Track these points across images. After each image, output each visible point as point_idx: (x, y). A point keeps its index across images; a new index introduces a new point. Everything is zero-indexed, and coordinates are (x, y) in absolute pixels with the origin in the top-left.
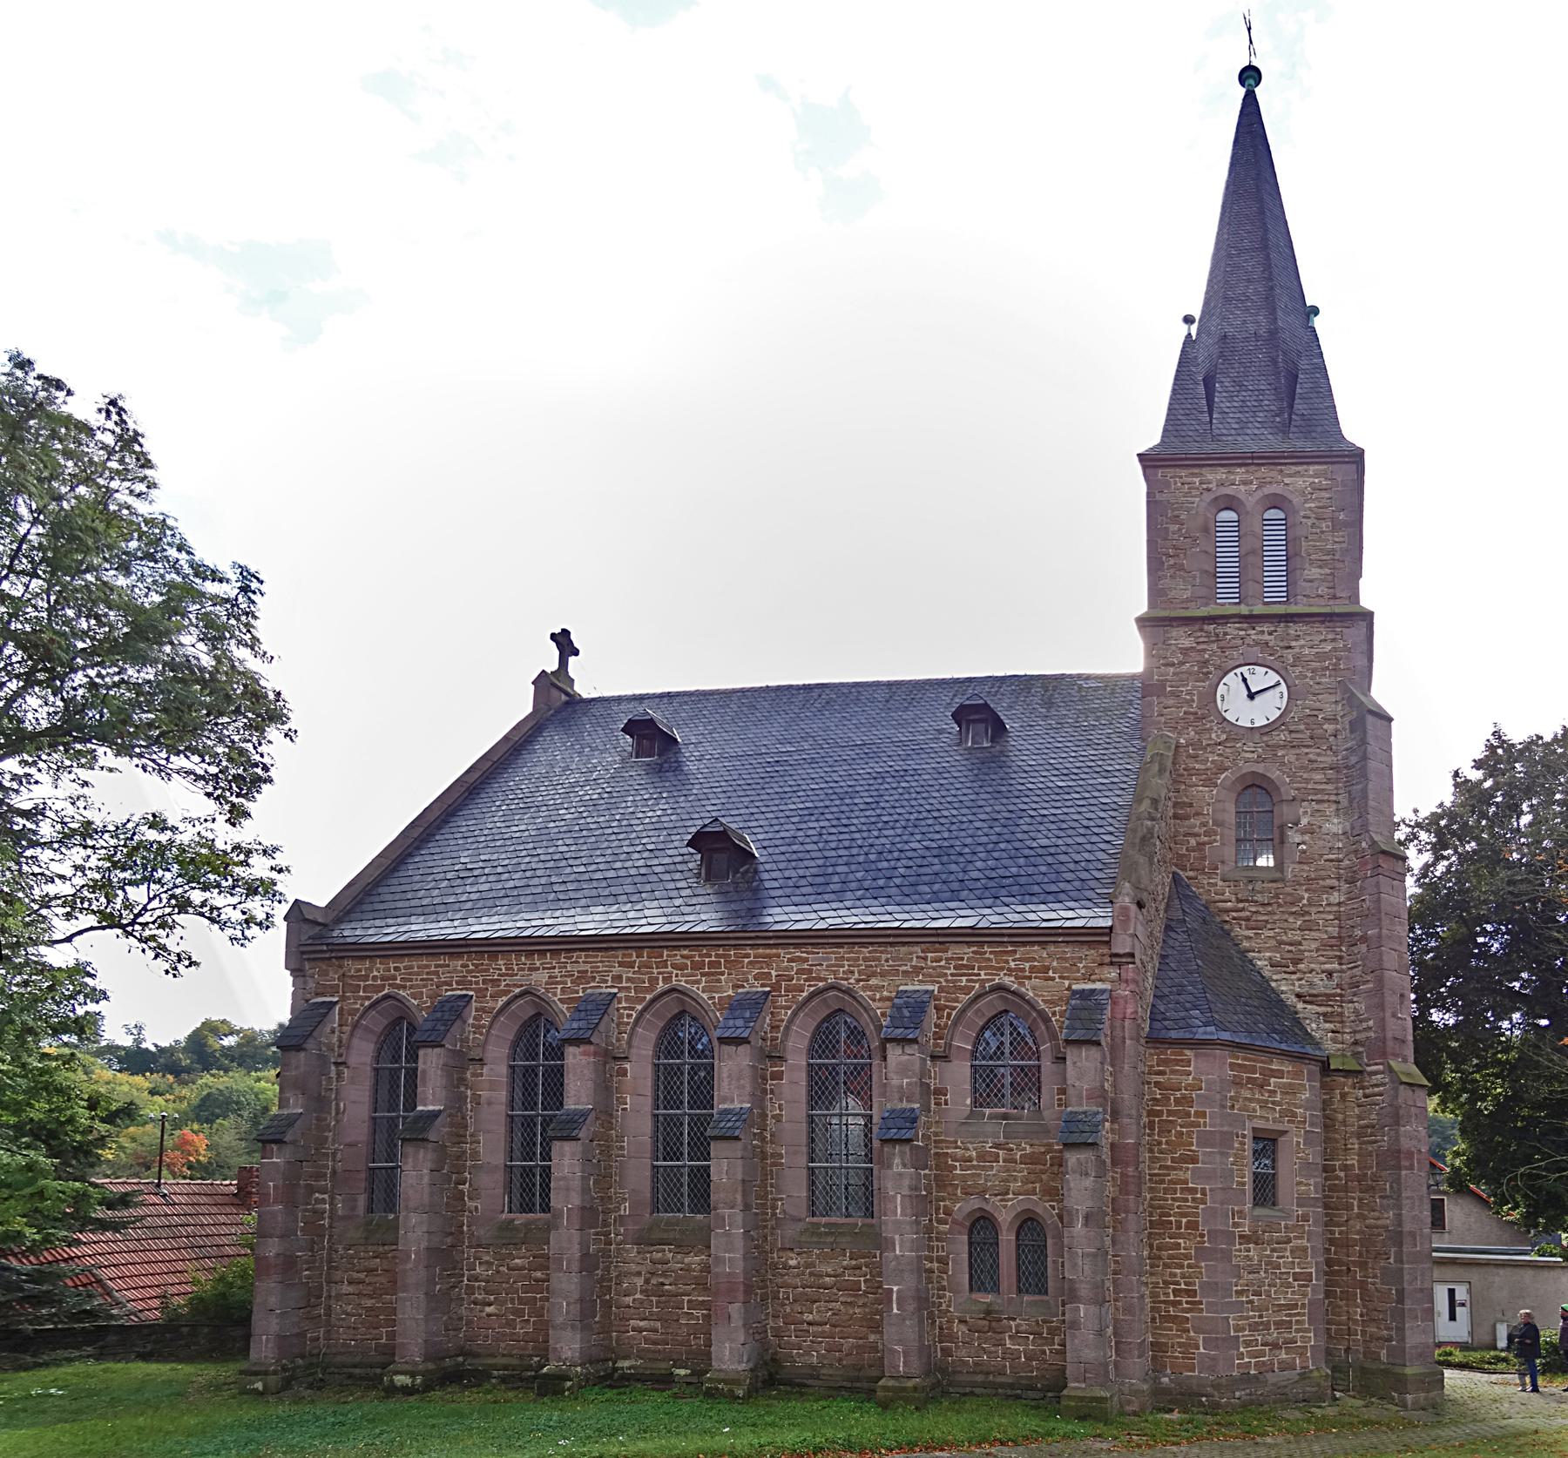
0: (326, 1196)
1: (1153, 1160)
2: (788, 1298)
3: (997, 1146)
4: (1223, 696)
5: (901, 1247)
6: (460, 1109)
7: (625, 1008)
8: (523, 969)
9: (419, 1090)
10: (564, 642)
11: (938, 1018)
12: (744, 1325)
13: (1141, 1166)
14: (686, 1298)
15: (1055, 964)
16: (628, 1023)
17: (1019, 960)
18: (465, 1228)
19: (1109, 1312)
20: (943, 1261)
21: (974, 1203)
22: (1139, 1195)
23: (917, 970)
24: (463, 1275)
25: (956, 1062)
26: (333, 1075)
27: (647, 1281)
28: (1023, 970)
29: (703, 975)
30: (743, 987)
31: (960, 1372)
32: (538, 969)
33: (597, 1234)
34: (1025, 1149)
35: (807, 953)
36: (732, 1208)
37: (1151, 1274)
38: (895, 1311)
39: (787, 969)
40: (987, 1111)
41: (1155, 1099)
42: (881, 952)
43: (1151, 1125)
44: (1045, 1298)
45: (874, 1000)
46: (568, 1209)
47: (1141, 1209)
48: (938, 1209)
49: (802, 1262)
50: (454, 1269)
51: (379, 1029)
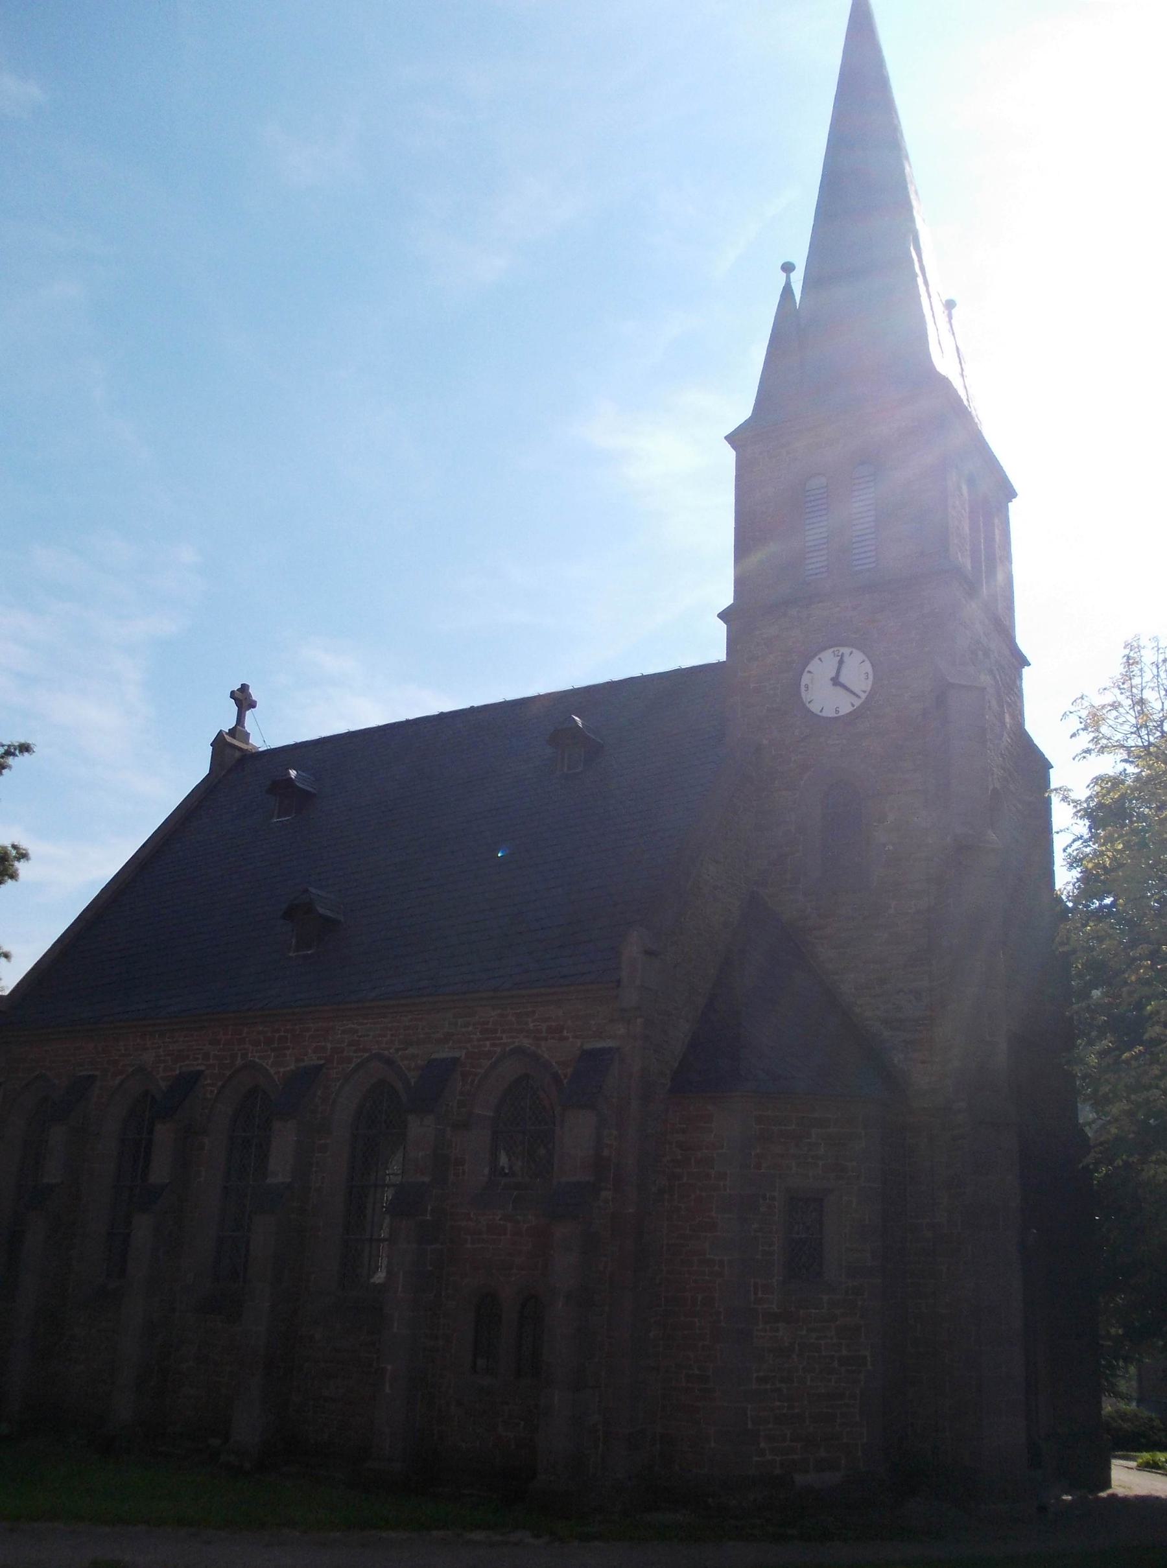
4: (807, 687)
10: (243, 699)
38: (388, 1390)
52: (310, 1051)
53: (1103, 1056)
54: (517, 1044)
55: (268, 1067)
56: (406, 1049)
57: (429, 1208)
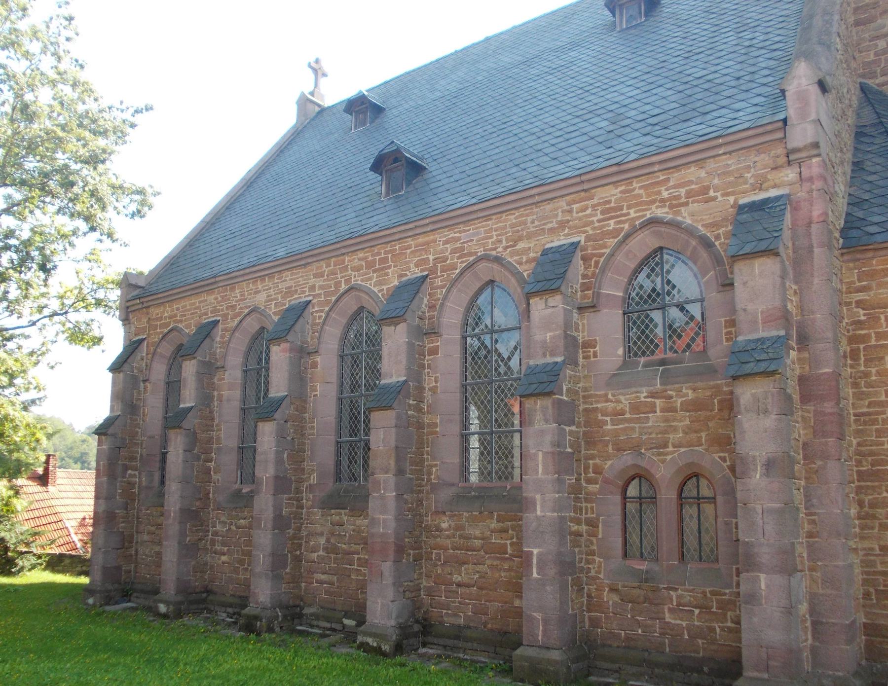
0: (137, 473)
1: (860, 396)
2: (440, 560)
3: (652, 395)
5: (542, 507)
6: (208, 405)
7: (317, 312)
8: (251, 294)
9: (182, 392)
10: (317, 70)
11: (586, 268)
12: (394, 584)
13: (843, 403)
14: (356, 556)
15: (716, 181)
16: (318, 324)
17: (674, 187)
18: (211, 495)
19: (801, 584)
20: (592, 524)
21: (627, 459)
22: (841, 438)
23: (562, 225)
24: (208, 531)
25: (604, 311)
26: (142, 389)
27: (328, 541)
28: (678, 197)
29: (374, 271)
30: (406, 275)
31: (610, 646)
32: (260, 292)
33: (290, 499)
34: (687, 395)
35: (460, 232)
36: (386, 472)
37: (863, 538)
38: (535, 575)
39: (442, 252)
40: (642, 360)
41: (860, 322)
42: (527, 215)
43: (854, 355)
44: (716, 566)
45: (520, 264)
46: (266, 478)
47: (844, 455)
48: (586, 468)
49: (453, 524)
50: (202, 525)
51: (168, 355)
52: (411, 265)
53: (349, 622)
54: (648, 216)
55: (372, 287)
56: (516, 246)
57: (565, 388)
